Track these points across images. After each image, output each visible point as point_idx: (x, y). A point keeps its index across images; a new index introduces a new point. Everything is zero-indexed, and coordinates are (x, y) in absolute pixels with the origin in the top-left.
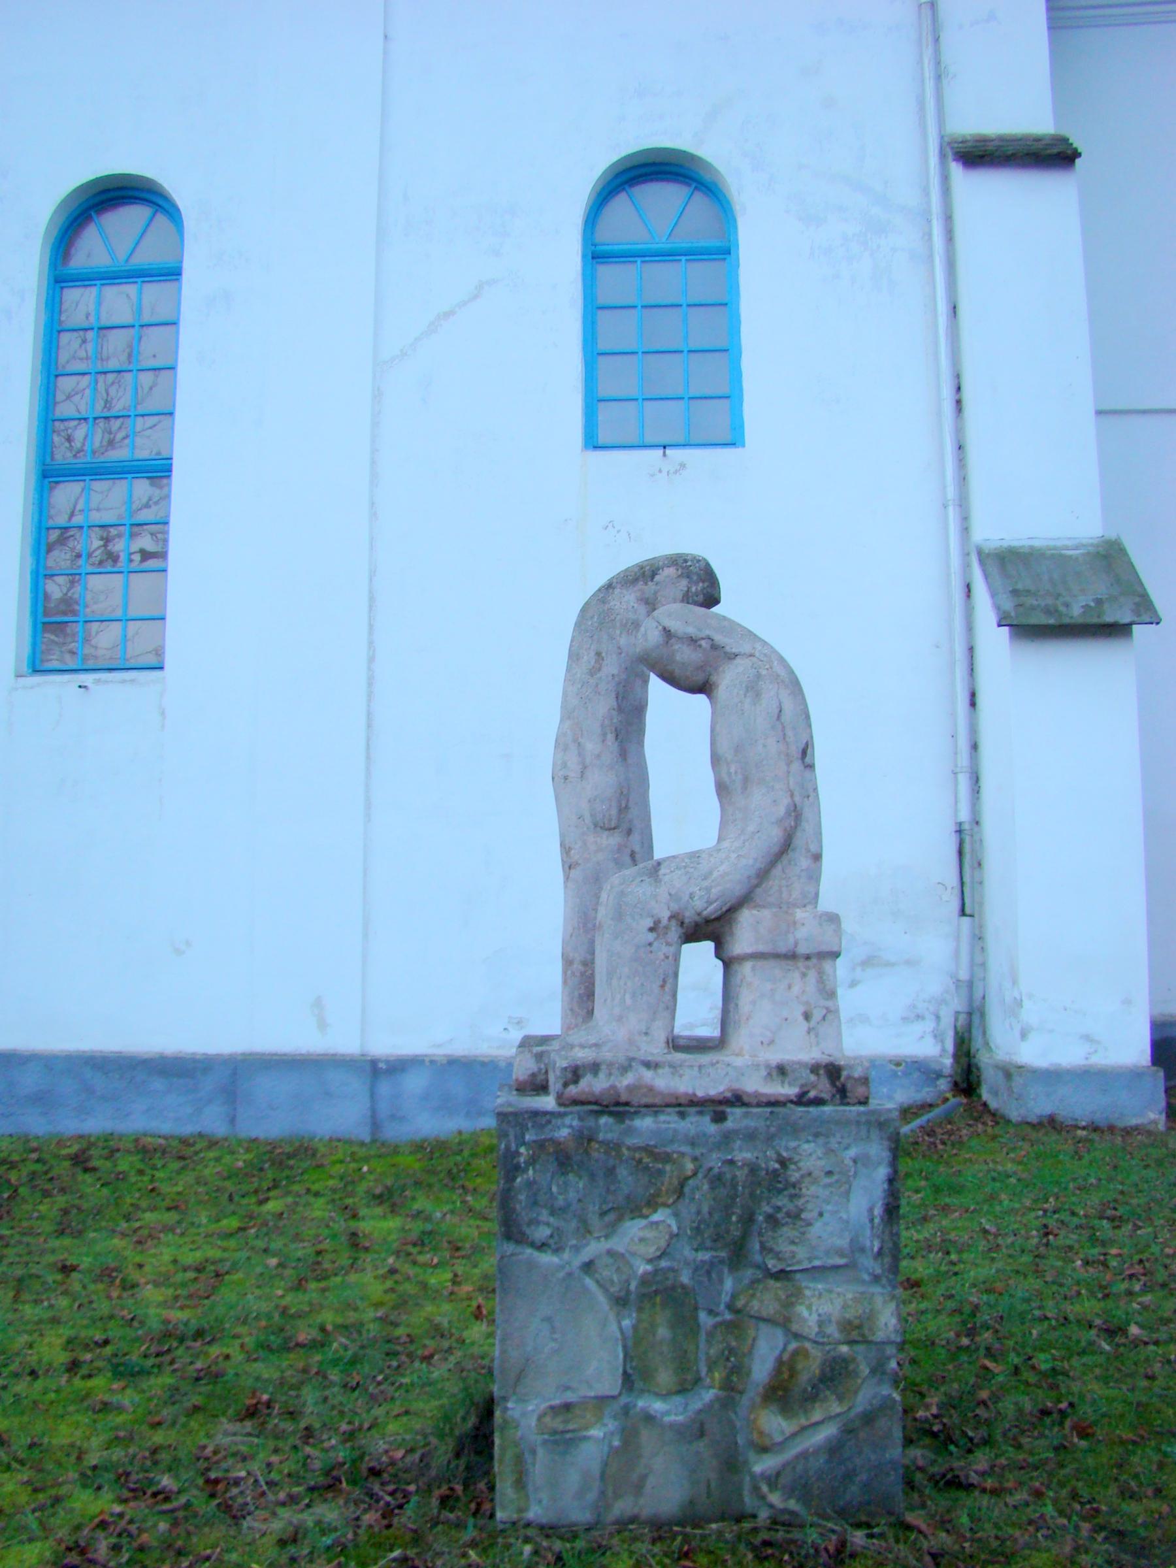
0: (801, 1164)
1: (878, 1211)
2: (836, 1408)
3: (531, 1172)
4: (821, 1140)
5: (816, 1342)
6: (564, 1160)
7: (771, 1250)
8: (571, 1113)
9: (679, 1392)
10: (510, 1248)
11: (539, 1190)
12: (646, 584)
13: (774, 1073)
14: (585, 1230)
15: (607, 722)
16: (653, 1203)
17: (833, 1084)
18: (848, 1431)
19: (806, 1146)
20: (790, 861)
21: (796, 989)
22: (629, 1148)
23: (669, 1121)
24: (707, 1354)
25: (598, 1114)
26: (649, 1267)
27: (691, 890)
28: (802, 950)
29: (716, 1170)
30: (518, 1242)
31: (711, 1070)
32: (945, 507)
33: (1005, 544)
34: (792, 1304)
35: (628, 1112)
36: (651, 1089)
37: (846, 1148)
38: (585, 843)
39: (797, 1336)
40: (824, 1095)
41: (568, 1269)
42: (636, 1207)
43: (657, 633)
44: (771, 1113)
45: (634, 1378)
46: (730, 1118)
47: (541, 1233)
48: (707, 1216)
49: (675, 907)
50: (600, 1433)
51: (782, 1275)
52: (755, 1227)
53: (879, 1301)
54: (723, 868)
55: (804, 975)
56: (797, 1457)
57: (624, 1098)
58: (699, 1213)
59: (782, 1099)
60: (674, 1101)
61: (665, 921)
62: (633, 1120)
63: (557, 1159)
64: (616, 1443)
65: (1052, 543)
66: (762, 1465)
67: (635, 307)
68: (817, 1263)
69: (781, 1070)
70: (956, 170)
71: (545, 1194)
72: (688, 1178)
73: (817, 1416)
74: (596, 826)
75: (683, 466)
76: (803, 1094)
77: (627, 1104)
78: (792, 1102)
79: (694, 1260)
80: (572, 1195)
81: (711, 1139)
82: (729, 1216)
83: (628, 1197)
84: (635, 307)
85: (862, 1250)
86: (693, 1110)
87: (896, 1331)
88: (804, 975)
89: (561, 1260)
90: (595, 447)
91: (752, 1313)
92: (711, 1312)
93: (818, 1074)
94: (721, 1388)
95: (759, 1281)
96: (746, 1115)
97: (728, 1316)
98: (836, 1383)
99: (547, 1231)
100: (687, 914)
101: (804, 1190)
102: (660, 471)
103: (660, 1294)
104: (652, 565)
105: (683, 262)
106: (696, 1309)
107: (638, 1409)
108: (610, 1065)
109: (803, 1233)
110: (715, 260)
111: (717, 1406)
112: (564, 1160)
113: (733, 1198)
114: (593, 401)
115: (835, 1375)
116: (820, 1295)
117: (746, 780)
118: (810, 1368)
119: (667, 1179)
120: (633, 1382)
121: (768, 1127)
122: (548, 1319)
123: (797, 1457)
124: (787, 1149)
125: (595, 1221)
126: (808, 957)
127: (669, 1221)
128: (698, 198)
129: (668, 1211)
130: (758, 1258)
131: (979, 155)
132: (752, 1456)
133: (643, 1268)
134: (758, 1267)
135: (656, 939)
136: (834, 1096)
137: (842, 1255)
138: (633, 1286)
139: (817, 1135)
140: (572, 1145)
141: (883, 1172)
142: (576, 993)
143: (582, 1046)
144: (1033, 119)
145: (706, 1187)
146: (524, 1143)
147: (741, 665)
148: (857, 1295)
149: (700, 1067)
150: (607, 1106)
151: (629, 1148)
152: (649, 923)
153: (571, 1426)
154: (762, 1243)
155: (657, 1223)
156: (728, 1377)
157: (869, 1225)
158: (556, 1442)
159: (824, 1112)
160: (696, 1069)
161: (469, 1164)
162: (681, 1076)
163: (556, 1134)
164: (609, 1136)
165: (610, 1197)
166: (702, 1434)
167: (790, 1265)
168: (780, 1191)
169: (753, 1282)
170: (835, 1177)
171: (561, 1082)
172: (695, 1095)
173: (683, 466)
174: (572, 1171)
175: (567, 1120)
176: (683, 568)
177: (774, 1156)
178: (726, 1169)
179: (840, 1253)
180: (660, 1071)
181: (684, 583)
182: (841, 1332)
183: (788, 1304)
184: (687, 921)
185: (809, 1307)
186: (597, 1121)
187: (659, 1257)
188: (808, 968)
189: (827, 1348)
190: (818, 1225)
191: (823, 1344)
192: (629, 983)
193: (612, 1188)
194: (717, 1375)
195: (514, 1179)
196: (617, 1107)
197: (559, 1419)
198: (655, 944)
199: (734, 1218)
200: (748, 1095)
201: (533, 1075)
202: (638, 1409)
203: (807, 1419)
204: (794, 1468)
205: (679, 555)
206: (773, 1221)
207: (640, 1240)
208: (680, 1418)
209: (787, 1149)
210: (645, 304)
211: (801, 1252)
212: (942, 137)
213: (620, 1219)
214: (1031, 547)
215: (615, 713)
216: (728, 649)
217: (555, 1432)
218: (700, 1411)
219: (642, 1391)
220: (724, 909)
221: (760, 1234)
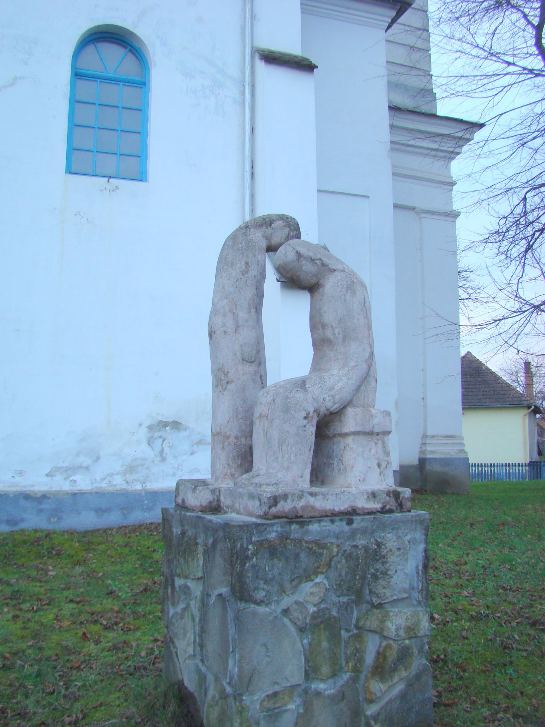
0: (387, 545)
1: (420, 568)
2: (404, 674)
3: (255, 559)
4: (395, 532)
5: (394, 640)
6: (272, 551)
7: (374, 593)
8: (277, 523)
9: (332, 677)
10: (242, 605)
11: (259, 570)
12: (267, 228)
13: (371, 497)
14: (282, 591)
15: (251, 302)
16: (316, 573)
17: (397, 502)
18: (410, 685)
19: (388, 535)
20: (367, 382)
21: (373, 451)
22: (306, 542)
23: (326, 525)
24: (346, 653)
25: (291, 523)
26: (315, 609)
27: (323, 396)
28: (376, 430)
29: (348, 551)
30: (247, 601)
31: (341, 496)
34: (385, 621)
35: (306, 521)
36: (313, 508)
37: (406, 535)
38: (237, 369)
39: (386, 638)
40: (393, 508)
41: (274, 614)
42: (307, 576)
43: (293, 254)
44: (374, 518)
45: (311, 672)
46: (355, 522)
47: (261, 595)
48: (344, 577)
49: (316, 405)
50: (293, 706)
51: (380, 606)
52: (366, 581)
53: (421, 614)
54: (340, 385)
55: (376, 444)
56: (387, 703)
57: (300, 514)
58: (340, 575)
59: (374, 510)
60: (324, 514)
61: (311, 413)
62: (308, 525)
63: (269, 551)
64: (301, 711)
66: (371, 710)
67: (95, 104)
68: (395, 598)
69: (374, 495)
70: (261, 65)
71: (263, 572)
72: (334, 557)
73: (396, 679)
74: (243, 360)
75: (117, 188)
76: (384, 507)
77: (301, 517)
78: (379, 512)
79: (339, 602)
80: (276, 571)
81: (346, 534)
82: (355, 576)
83: (305, 570)
84: (95, 104)
85: (413, 588)
86: (337, 518)
87: (428, 630)
88: (376, 444)
89: (270, 609)
90: (70, 173)
91: (366, 628)
92: (348, 630)
93: (390, 496)
94: (352, 672)
95: (369, 610)
96: (363, 519)
97: (355, 631)
98: (404, 660)
99: (264, 593)
100: (322, 410)
101: (389, 559)
103: (322, 623)
104: (269, 218)
106: (340, 629)
107: (312, 690)
108: (293, 495)
109: (389, 582)
111: (350, 682)
112: (272, 551)
113: (357, 566)
114: (72, 149)
115: (404, 655)
116: (397, 614)
117: (345, 338)
118: (392, 655)
119: (324, 559)
120: (309, 675)
121: (372, 526)
122: (265, 645)
123: (387, 703)
124: (380, 537)
125: (287, 585)
126: (378, 434)
127: (324, 582)
129: (323, 576)
130: (368, 598)
131: (272, 58)
132: (365, 706)
133: (312, 609)
134: (368, 602)
135: (308, 423)
136: (397, 508)
137: (406, 592)
138: (308, 621)
139: (393, 529)
140: (277, 542)
141: (422, 547)
142: (231, 455)
143: (268, 485)
144: (292, 46)
145: (343, 561)
146: (252, 543)
147: (338, 276)
148: (413, 613)
149: (336, 494)
150: (291, 519)
151: (306, 542)
152: (304, 414)
153: (277, 705)
154: (369, 589)
155: (318, 584)
156: (356, 665)
157: (416, 575)
158: (270, 716)
159: (397, 516)
160: (335, 495)
161: (14, 551)
162: (327, 500)
163: (269, 536)
164: (296, 536)
165: (296, 571)
166: (343, 698)
167: (383, 600)
168: (377, 560)
169: (368, 610)
170: (402, 551)
171: (268, 506)
172: (334, 510)
173: (117, 188)
174: (276, 557)
175: (275, 528)
176: (286, 222)
177: (374, 542)
178: (353, 550)
179: (405, 591)
180: (317, 497)
181: (287, 230)
182: (406, 633)
183: (383, 621)
184: (321, 413)
185: (392, 622)
186: (290, 528)
187: (320, 602)
188: (378, 440)
189: (400, 642)
190: (395, 577)
191: (397, 640)
192: (293, 449)
193: (298, 565)
194: (350, 664)
195: (245, 563)
196: (297, 518)
197: (271, 702)
198: (307, 426)
199: (357, 577)
200: (359, 509)
201: (210, 502)
202: (312, 690)
203: (392, 681)
204: (385, 709)
205: (284, 215)
206: (375, 577)
207: (311, 593)
208: (333, 691)
209: (380, 537)
210: (100, 103)
211: (388, 592)
212: (253, 48)
213: (300, 583)
215: (255, 297)
216: (330, 266)
217: (269, 710)
218: (343, 685)
219: (314, 679)
220: (341, 407)
221: (369, 585)
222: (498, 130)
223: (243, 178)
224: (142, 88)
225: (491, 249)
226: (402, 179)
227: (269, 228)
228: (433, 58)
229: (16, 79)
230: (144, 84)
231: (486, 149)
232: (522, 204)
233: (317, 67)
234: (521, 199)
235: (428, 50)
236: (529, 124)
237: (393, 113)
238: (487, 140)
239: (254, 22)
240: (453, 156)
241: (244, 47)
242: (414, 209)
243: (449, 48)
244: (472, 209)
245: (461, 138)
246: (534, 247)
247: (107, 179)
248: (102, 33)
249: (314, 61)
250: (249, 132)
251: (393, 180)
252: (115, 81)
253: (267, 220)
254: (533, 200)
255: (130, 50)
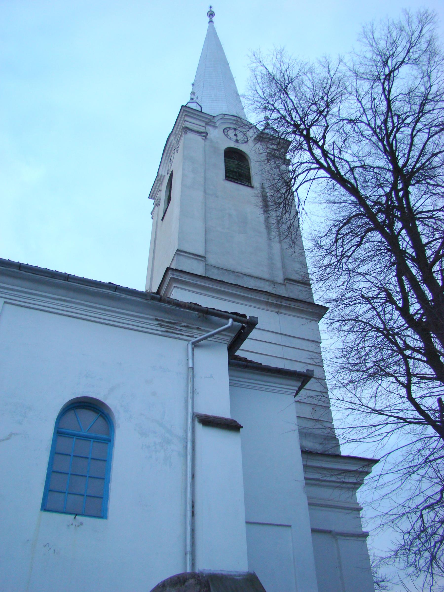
12: (181, 586)
32: (186, 554)
33: (212, 572)
65: (229, 573)
67: (70, 455)
70: (199, 427)
75: (82, 524)
84: (70, 455)
102: (72, 524)
105: (92, 442)
110: (84, 439)
114: (49, 490)
128: (101, 419)
131: (208, 421)
144: (223, 411)
173: (82, 524)
212: (193, 413)
214: (222, 574)
222: (388, 467)
223: (185, 516)
224: (107, 443)
225: (401, 562)
226: (318, 508)
227: (183, 586)
228: (333, 413)
229: (11, 435)
230: (110, 441)
231: (381, 481)
232: (419, 522)
233: (242, 427)
234: (418, 516)
235: (329, 407)
236: (411, 460)
237: (306, 456)
238: (381, 475)
239: (195, 395)
240: (356, 486)
241: (187, 414)
242: (329, 532)
243: (342, 406)
244: (377, 532)
245: (362, 472)
246: (437, 557)
247: (74, 516)
248: (80, 402)
249: (240, 423)
250: (190, 478)
251: (309, 509)
252: (87, 438)
253: (181, 578)
254: (429, 516)
255: (101, 415)
